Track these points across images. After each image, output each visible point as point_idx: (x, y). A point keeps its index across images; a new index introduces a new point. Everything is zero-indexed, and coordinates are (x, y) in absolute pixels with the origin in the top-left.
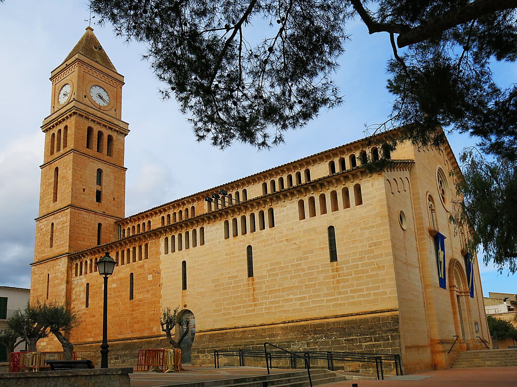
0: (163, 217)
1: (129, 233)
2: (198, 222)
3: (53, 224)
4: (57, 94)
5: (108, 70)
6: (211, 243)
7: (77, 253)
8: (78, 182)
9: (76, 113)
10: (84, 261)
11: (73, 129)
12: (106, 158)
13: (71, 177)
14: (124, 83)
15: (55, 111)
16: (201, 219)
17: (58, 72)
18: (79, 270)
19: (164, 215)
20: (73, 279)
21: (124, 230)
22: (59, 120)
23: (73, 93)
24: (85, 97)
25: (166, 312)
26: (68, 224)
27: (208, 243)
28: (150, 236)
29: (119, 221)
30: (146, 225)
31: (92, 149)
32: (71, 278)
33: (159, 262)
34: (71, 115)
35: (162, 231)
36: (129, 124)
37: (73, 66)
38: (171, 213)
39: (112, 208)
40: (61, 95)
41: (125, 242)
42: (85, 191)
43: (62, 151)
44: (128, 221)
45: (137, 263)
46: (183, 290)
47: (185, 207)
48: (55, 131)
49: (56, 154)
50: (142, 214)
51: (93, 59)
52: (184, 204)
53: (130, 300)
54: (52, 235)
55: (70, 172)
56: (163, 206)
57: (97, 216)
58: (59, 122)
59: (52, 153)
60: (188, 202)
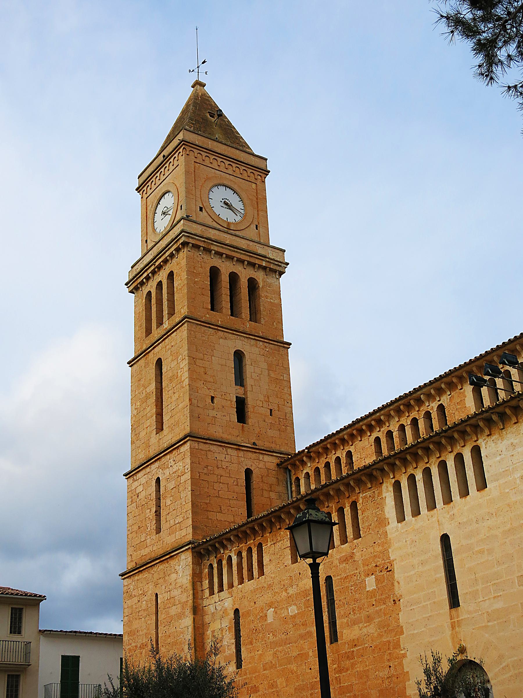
0: (378, 440)
1: (308, 484)
2: (463, 434)
3: (158, 480)
4: (150, 215)
5: (238, 151)
6: (502, 481)
7: (211, 540)
8: (200, 384)
9: (188, 243)
10: (226, 557)
11: (184, 275)
12: (249, 326)
13: (186, 375)
14: (269, 172)
15: (149, 247)
16: (471, 425)
17: (150, 173)
18: (216, 580)
19: (380, 435)
20: (205, 602)
21: (298, 480)
22: (157, 264)
23: (178, 207)
24: (201, 209)
25: (431, 665)
26: (188, 476)
27: (496, 484)
28: (359, 482)
29: (286, 461)
30: (343, 461)
31: (220, 311)
32: (202, 599)
33: (386, 543)
34: (178, 250)
35: (386, 468)
36: (284, 251)
37: (176, 155)
38: (394, 427)
39: (270, 433)
40: (158, 216)
41: (348, 485)
42: (215, 400)
43: (166, 325)
44: (305, 458)
45: (338, 552)
46: (450, 609)
47: (424, 409)
48: (151, 286)
49: (156, 333)
50: (333, 439)
51: (209, 136)
52: (419, 402)
54: (158, 506)
55: (184, 364)
56: (375, 412)
57: (241, 454)
58: (157, 267)
59: (148, 331)
60: (430, 396)
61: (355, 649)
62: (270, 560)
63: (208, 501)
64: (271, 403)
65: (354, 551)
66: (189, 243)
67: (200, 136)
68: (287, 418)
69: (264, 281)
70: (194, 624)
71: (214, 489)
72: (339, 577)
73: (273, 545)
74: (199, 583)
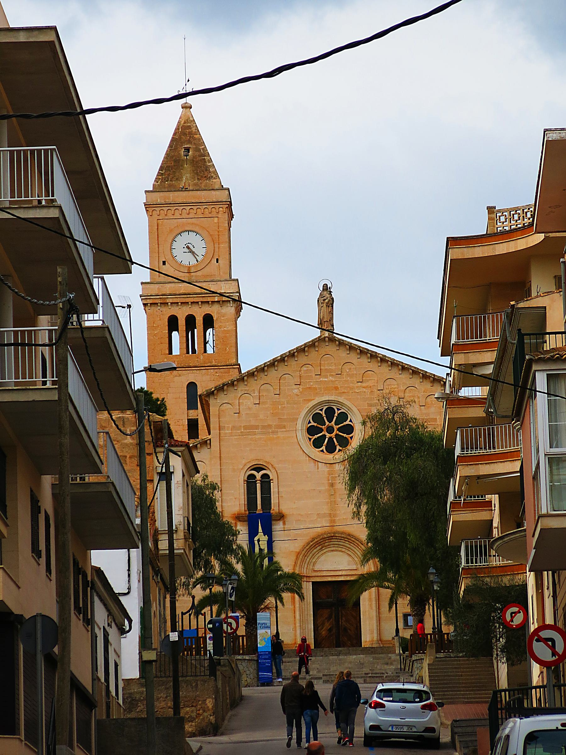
24: (164, 263)
66: (147, 304)
67: (162, 193)
69: (218, 313)
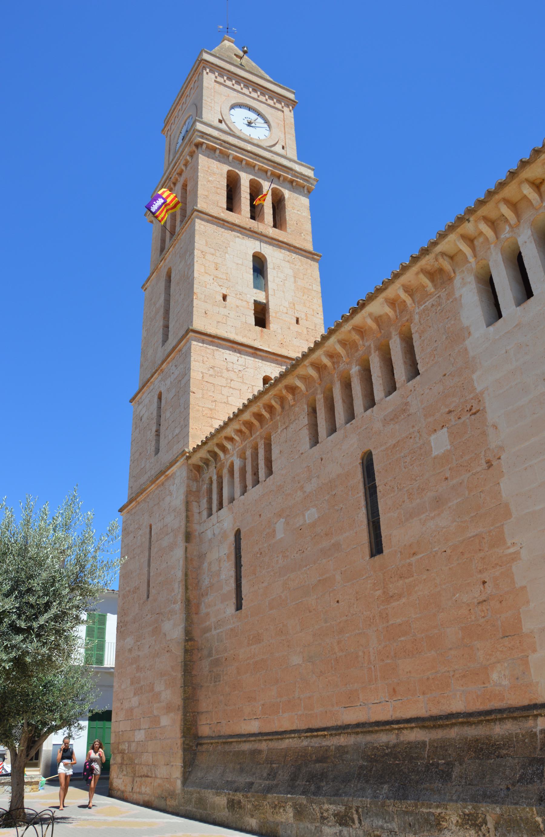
18: (215, 497)
42: (228, 299)
53: (372, 555)
61: (413, 559)
62: (281, 452)
63: (213, 407)
64: (297, 311)
65: (409, 400)
68: (317, 329)
70: (186, 554)
71: (221, 394)
72: (383, 448)
73: (285, 430)
74: (196, 503)
